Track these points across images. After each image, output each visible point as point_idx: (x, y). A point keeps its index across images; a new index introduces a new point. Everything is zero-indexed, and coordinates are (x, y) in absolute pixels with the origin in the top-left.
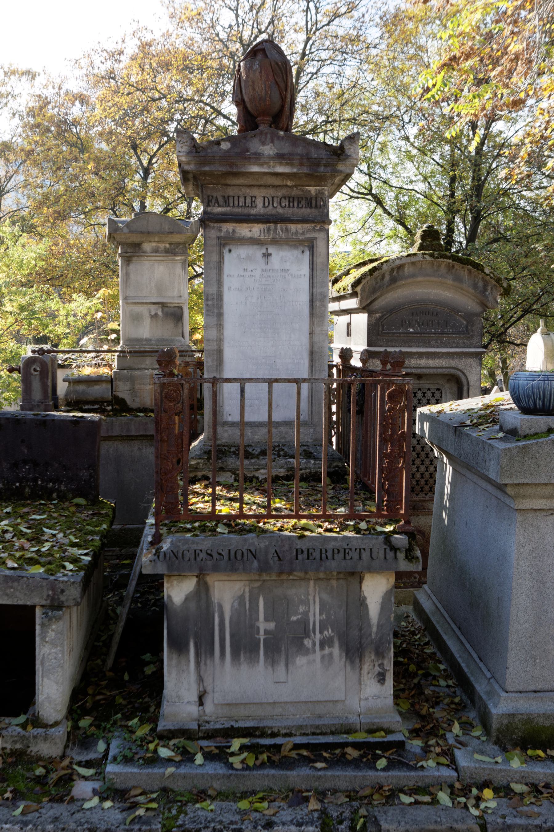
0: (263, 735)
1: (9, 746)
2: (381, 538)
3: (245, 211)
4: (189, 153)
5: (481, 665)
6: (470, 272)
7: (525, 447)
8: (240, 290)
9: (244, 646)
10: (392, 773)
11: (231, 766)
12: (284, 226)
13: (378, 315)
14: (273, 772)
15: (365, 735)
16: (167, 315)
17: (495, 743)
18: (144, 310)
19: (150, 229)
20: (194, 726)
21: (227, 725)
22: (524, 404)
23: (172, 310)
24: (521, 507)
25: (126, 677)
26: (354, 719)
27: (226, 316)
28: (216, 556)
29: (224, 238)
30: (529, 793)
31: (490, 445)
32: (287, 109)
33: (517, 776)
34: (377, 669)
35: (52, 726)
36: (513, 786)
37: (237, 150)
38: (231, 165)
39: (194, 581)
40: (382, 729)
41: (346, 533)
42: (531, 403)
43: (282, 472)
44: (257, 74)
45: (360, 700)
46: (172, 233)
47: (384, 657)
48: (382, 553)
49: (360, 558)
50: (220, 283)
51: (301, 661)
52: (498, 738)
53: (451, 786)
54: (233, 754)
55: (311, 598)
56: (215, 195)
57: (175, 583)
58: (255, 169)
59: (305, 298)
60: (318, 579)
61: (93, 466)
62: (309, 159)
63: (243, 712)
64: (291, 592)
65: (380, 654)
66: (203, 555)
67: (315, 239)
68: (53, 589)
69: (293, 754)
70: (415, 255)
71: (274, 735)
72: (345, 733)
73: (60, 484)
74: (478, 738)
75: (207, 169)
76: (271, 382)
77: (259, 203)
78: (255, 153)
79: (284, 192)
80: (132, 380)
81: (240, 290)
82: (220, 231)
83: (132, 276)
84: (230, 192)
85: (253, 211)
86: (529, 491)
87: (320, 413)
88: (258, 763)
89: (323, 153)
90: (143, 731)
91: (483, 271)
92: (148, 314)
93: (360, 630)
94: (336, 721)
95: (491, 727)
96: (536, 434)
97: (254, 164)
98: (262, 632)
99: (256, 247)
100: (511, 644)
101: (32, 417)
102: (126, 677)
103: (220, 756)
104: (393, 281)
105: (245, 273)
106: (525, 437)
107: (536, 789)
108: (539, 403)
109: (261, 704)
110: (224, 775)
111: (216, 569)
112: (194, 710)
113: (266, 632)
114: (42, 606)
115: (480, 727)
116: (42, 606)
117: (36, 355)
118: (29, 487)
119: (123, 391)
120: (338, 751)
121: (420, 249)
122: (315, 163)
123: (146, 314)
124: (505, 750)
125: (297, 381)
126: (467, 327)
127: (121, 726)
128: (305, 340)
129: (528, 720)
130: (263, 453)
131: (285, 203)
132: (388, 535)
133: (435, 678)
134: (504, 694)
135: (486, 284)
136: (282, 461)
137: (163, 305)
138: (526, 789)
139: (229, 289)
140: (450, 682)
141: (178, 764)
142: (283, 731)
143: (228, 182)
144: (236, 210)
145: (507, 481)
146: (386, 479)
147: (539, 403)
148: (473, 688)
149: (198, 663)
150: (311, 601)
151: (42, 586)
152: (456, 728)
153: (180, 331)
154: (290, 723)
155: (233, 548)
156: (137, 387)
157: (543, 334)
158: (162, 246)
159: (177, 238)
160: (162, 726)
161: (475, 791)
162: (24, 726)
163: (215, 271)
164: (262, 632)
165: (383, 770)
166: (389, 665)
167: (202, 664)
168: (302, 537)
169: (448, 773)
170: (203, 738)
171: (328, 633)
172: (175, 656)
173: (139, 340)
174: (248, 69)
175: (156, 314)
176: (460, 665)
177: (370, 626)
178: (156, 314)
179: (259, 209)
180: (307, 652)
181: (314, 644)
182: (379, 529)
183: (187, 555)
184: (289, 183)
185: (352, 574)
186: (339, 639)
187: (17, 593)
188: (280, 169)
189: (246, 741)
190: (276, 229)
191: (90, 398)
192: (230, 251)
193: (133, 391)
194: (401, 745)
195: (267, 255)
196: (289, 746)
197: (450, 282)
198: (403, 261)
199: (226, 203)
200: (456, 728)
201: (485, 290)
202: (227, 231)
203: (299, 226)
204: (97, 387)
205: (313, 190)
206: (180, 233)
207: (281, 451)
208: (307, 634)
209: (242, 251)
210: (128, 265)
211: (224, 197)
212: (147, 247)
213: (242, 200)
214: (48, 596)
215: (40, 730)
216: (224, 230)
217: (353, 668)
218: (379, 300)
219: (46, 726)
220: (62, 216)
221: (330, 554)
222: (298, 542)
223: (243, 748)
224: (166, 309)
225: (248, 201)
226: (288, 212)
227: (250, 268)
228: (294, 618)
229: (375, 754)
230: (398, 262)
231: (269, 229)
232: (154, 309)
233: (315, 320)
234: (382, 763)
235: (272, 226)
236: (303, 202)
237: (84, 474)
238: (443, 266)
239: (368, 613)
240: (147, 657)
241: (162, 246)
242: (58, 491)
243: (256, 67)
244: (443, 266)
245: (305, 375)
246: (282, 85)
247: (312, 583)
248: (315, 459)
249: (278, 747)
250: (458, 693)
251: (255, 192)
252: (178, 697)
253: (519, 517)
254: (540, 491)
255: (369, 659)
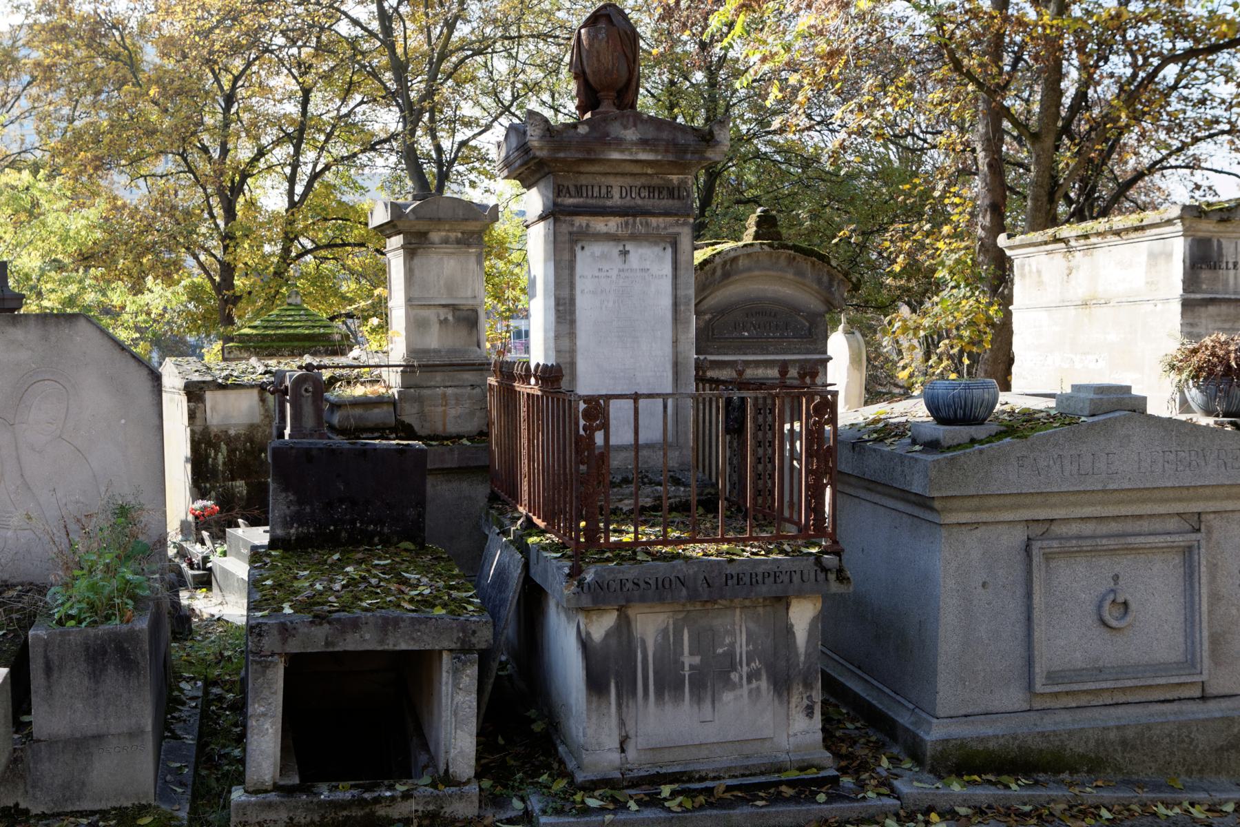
0: (691, 779)
1: (420, 808)
2: (812, 558)
3: (600, 202)
4: (542, 137)
5: (898, 698)
6: (813, 264)
7: (953, 458)
8: (594, 293)
9: (669, 684)
10: (834, 805)
11: (669, 810)
12: (643, 219)
13: (707, 317)
14: (715, 812)
15: (797, 773)
16: (458, 320)
17: (930, 772)
18: (430, 314)
19: (441, 215)
20: (618, 775)
21: (653, 771)
22: (943, 414)
23: (465, 313)
24: (947, 521)
25: (501, 741)
26: (783, 757)
27: (578, 324)
28: (642, 585)
29: (578, 233)
30: (974, 814)
31: (912, 458)
32: (634, 84)
33: (960, 800)
34: (806, 702)
35: (465, 784)
36: (957, 808)
37: (595, 134)
38: (589, 151)
39: (615, 614)
40: (813, 766)
41: (772, 556)
42: (952, 413)
43: (648, 502)
44: (604, 44)
45: (788, 736)
46: (466, 220)
47: (812, 689)
48: (813, 574)
49: (791, 581)
50: (572, 286)
51: (728, 696)
52: (932, 766)
53: (897, 815)
54: (665, 799)
55: (737, 627)
56: (566, 184)
57: (594, 618)
58: (616, 156)
59: (667, 302)
60: (744, 607)
61: (421, 503)
62: (676, 145)
63: (668, 756)
64: (717, 623)
65: (808, 685)
66: (629, 585)
67: (679, 234)
68: (464, 631)
69: (728, 795)
70: (752, 245)
71: (702, 779)
72: (775, 772)
73: (383, 525)
74: (910, 769)
75: (562, 155)
76: (636, 397)
77: (616, 193)
78: (616, 138)
79: (643, 180)
80: (420, 400)
81: (594, 293)
82: (573, 225)
83: (417, 272)
84: (583, 180)
85: (609, 203)
86: (956, 503)
87: (686, 434)
88: (697, 805)
89: (691, 139)
90: (561, 784)
91: (829, 263)
92: (436, 320)
93: (788, 660)
94: (765, 761)
95: (925, 755)
96: (959, 445)
97: (615, 150)
98: (687, 667)
99: (612, 243)
100: (940, 667)
101: (348, 446)
102: (501, 741)
103: (653, 801)
104: (726, 275)
105: (600, 274)
106: (948, 448)
107: (980, 811)
108: (960, 413)
109: (687, 746)
110: (665, 818)
111: (643, 599)
112: (616, 757)
113: (692, 667)
114: (451, 650)
115: (908, 759)
116: (451, 650)
117: (304, 371)
118: (346, 531)
119: (409, 415)
120: (772, 791)
121: (756, 238)
122: (682, 150)
123: (434, 319)
124: (940, 778)
125: (664, 397)
126: (810, 329)
127: (532, 783)
128: (668, 349)
129: (962, 744)
130: (626, 481)
131: (644, 193)
132: (817, 557)
133: (839, 721)
134: (935, 720)
135: (831, 279)
136: (648, 490)
137: (454, 308)
138: (970, 811)
139: (582, 291)
140: (858, 725)
141: (614, 812)
142: (712, 775)
143: (582, 169)
144: (590, 201)
145: (935, 494)
146: (813, 496)
147: (960, 413)
148: (894, 721)
149: (619, 706)
150: (738, 632)
151: (452, 628)
152: (885, 763)
153: (475, 339)
154: (718, 765)
155: (660, 576)
156: (426, 410)
157: (846, 332)
158: (453, 235)
159: (472, 226)
160: (580, 777)
161: (920, 817)
162: (434, 785)
163: (567, 272)
164: (687, 667)
165: (825, 803)
166: (817, 695)
167: (624, 709)
168: (732, 561)
169: (890, 802)
170: (628, 787)
171: (756, 665)
172: (595, 699)
173: (426, 352)
174: (592, 38)
175: (446, 319)
176: (870, 704)
177: (797, 655)
178: (446, 319)
179: (616, 200)
180: (733, 686)
181: (741, 678)
182: (805, 550)
183: (614, 585)
184: (649, 171)
185: (778, 599)
186: (767, 672)
187: (425, 637)
188: (643, 156)
189: (675, 786)
190: (635, 222)
191: (370, 424)
192: (583, 248)
193: (422, 415)
194: (834, 781)
195: (625, 253)
196: (722, 788)
197: (790, 276)
198: (739, 253)
199: (579, 192)
200: (885, 763)
201: (831, 286)
202: (580, 226)
203: (661, 219)
204: (376, 411)
205: (675, 178)
206: (476, 219)
207: (644, 478)
208: (733, 667)
209: (597, 249)
210: (412, 259)
211: (576, 186)
212: (435, 236)
213: (596, 189)
214: (459, 638)
215: (453, 789)
216: (577, 224)
217: (781, 702)
218: (709, 299)
219: (459, 784)
220: (100, 164)
221: (760, 578)
222: (728, 566)
223: (674, 794)
224: (457, 313)
225: (604, 191)
226: (649, 203)
227: (605, 268)
228: (720, 651)
229: (811, 791)
230: (732, 254)
231: (627, 224)
232: (443, 313)
233: (680, 327)
234: (821, 797)
235: (631, 219)
236: (665, 192)
237: (411, 513)
238: (783, 258)
239: (795, 642)
240: (532, 713)
241: (453, 235)
242: (380, 534)
243: (602, 35)
244: (783, 258)
245: (669, 390)
246: (630, 56)
247: (738, 611)
248: (685, 485)
249: (709, 791)
250: (871, 733)
251: (611, 180)
252: (599, 744)
253: (944, 532)
254: (968, 503)
255: (797, 689)
